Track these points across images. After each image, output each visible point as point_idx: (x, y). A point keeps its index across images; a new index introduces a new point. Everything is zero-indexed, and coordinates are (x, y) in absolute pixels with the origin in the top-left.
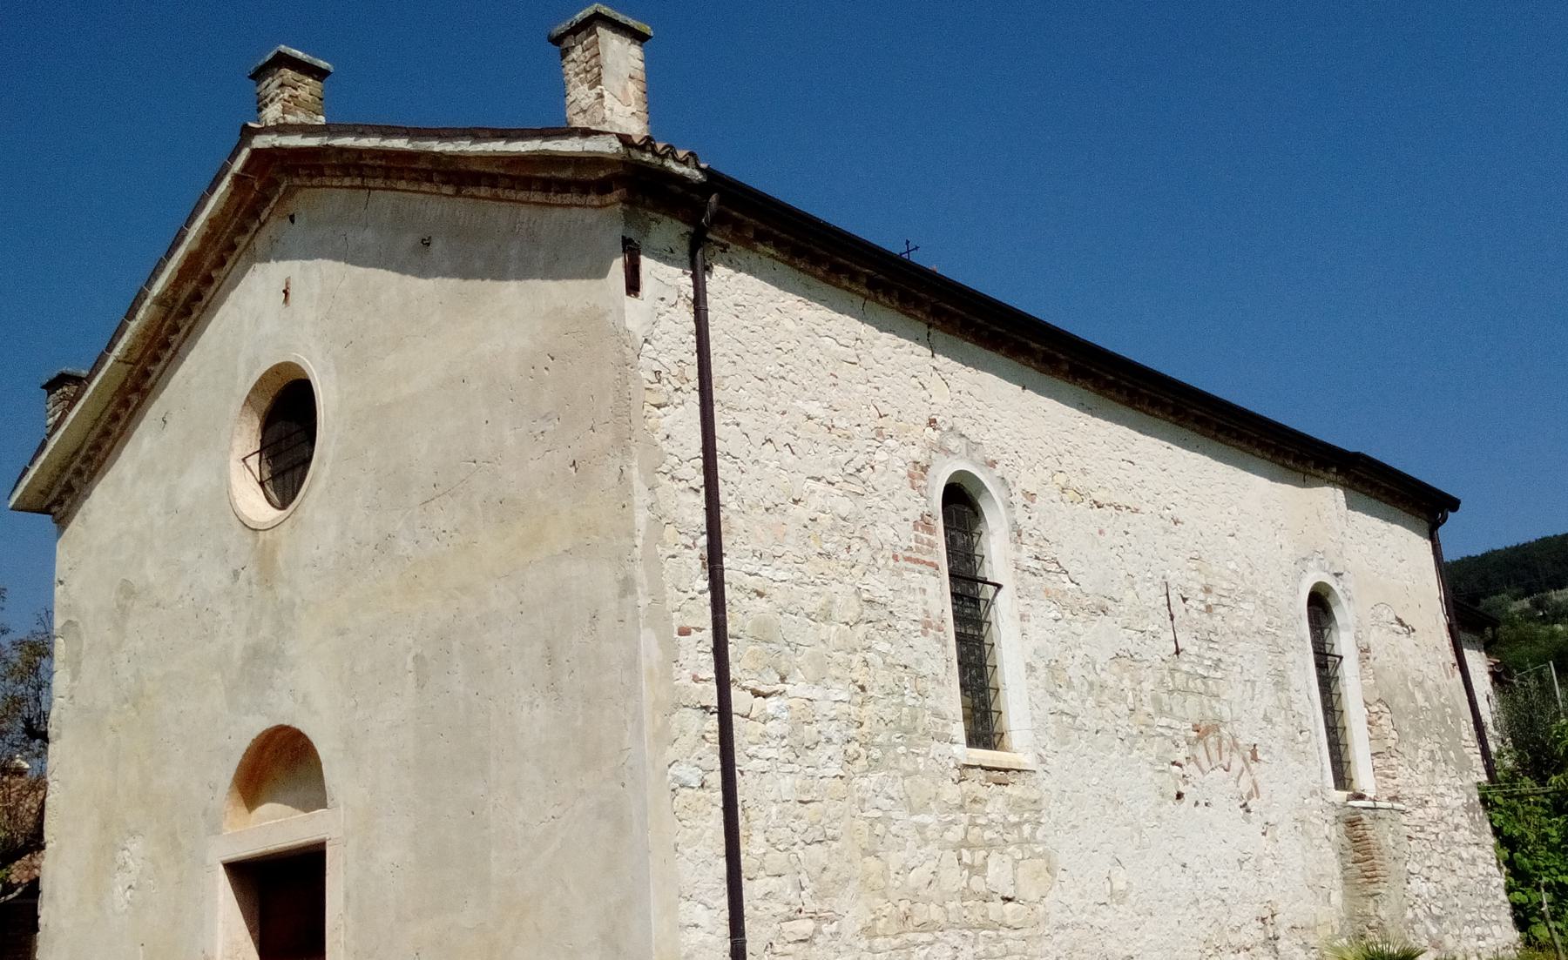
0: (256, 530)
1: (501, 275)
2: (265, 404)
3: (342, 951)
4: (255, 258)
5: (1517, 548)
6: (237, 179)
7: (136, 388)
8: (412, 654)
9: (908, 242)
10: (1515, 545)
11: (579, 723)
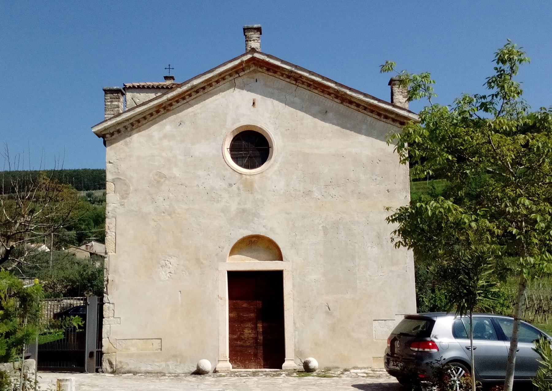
0: (241, 174)
1: (359, 132)
2: (236, 134)
3: (292, 300)
4: (234, 86)
5: (75, 171)
6: (242, 62)
7: (164, 108)
8: (321, 225)
9: (169, 65)
10: (73, 169)
11: (390, 254)
